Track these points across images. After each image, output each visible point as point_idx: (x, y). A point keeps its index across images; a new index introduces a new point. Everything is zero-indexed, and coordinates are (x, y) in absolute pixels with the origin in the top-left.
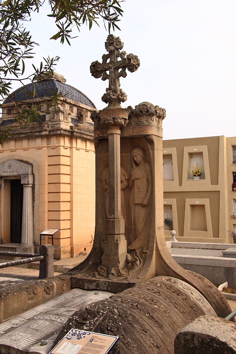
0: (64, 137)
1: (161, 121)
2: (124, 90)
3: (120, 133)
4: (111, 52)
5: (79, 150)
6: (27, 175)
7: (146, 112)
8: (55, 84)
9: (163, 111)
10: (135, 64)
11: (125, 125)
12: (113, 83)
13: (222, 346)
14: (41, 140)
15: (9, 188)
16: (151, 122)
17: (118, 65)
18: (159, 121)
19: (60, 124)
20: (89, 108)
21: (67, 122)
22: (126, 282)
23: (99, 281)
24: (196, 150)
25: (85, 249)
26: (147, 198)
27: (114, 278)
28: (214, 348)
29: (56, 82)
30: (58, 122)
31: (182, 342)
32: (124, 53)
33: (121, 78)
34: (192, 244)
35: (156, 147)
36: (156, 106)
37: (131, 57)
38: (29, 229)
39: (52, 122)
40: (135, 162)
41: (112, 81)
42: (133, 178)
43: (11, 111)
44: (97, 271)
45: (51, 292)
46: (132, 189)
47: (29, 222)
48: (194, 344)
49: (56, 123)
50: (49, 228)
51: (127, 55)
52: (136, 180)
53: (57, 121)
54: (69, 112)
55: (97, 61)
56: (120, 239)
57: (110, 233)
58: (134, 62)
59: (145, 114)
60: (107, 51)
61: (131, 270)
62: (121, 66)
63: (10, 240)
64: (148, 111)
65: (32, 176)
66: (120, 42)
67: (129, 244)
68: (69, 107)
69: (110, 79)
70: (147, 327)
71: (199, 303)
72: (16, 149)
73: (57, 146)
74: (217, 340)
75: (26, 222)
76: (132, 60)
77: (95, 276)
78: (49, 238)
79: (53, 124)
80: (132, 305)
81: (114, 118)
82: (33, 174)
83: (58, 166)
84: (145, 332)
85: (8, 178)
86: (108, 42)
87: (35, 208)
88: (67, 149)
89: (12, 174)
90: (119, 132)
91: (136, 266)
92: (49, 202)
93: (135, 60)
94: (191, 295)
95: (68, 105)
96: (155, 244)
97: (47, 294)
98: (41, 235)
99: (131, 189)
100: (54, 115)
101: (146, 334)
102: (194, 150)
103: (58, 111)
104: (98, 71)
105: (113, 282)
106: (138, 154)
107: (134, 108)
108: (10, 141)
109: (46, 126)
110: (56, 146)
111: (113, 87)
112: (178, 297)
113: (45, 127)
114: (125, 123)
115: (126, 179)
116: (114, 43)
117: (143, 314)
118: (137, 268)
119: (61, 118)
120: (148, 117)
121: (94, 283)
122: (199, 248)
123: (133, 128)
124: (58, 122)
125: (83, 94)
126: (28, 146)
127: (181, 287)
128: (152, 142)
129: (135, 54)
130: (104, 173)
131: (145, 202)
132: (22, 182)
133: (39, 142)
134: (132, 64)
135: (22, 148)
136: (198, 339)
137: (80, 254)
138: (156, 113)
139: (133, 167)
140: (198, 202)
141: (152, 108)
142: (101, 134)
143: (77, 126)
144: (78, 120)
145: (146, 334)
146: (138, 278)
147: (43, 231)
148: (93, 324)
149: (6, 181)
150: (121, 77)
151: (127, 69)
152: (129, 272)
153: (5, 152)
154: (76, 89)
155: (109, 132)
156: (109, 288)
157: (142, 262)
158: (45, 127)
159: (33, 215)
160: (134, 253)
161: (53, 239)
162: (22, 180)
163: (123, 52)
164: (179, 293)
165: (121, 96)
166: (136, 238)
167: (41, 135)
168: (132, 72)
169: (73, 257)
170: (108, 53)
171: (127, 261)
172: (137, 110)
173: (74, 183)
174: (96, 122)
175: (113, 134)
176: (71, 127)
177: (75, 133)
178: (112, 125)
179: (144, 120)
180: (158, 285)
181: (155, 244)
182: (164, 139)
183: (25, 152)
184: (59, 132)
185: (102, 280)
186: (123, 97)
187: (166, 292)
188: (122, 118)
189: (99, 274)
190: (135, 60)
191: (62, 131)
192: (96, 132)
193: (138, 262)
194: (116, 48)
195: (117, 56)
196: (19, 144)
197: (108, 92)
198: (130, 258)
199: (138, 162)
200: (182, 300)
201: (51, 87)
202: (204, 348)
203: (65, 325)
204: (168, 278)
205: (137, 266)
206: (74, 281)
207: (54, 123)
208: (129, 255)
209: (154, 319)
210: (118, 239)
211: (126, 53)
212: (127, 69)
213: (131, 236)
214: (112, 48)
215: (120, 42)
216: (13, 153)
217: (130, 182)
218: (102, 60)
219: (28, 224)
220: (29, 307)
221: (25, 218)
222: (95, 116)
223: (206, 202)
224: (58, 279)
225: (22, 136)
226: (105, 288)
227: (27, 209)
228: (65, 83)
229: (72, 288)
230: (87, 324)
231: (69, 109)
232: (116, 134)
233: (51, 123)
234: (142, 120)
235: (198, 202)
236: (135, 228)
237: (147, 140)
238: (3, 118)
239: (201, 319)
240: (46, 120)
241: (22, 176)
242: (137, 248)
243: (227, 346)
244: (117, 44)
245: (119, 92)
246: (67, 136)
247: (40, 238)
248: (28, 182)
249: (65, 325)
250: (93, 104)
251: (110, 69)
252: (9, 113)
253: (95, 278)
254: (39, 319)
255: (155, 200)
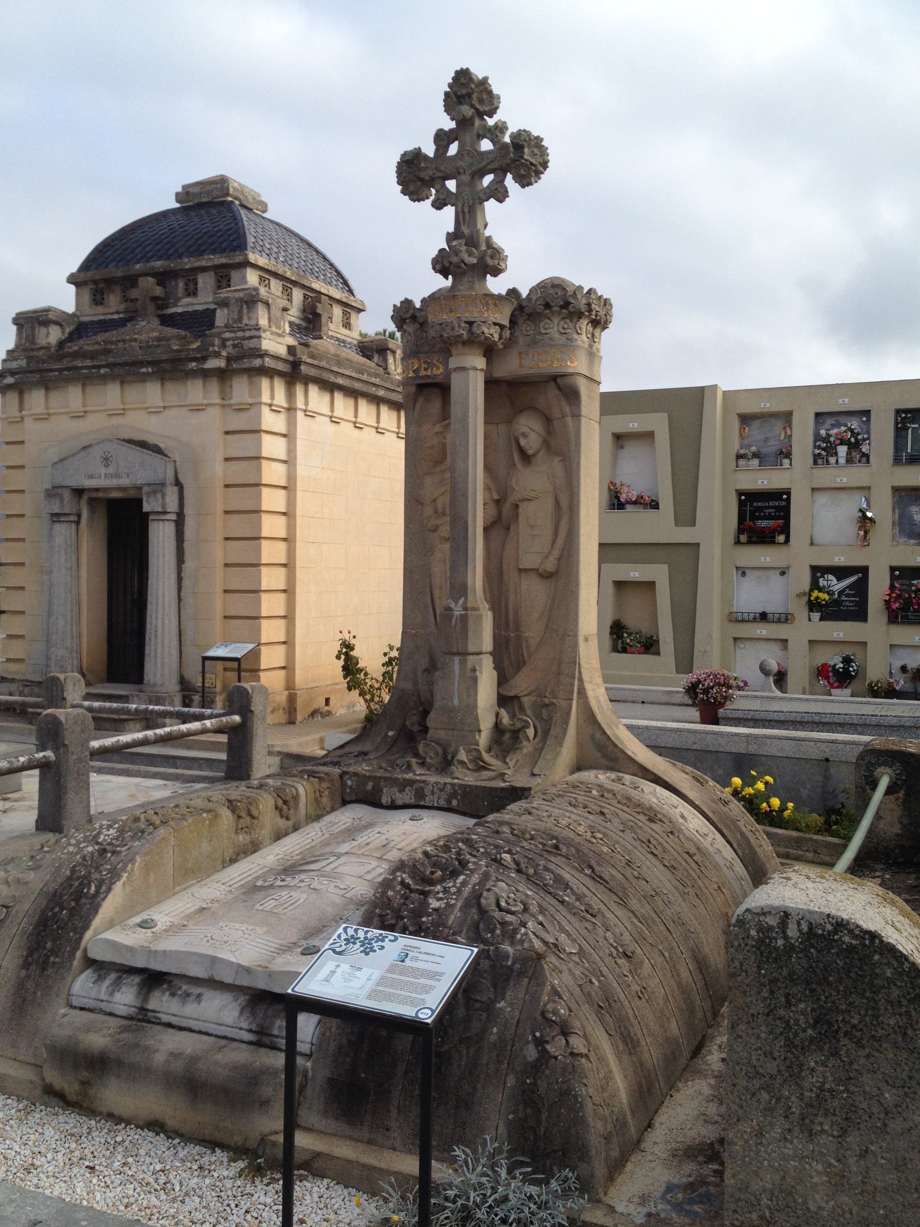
0: (271, 378)
1: (597, 334)
2: (499, 241)
3: (485, 368)
4: (463, 123)
5: (313, 417)
6: (158, 487)
7: (562, 307)
8: (238, 217)
9: (605, 305)
10: (533, 161)
11: (501, 346)
12: (467, 219)
13: (867, 942)
14: (204, 385)
15: (102, 525)
16: (576, 336)
17: (484, 163)
18: (593, 335)
19: (259, 337)
20: (337, 294)
21: (280, 332)
22: (503, 785)
23: (424, 782)
24: (636, 425)
25: (327, 701)
26: (556, 553)
27: (466, 775)
28: (844, 946)
29: (243, 212)
30: (254, 333)
31: (753, 933)
32: (501, 128)
33: (491, 205)
34: (624, 689)
35: (584, 410)
36: (590, 290)
37: (525, 141)
38: (166, 641)
39: (235, 332)
40: (522, 452)
41: (466, 210)
42: (512, 498)
43: (103, 294)
44: (416, 755)
45: (292, 811)
46: (512, 528)
47: (166, 622)
48: (786, 937)
49: (248, 334)
50: (226, 642)
51: (512, 133)
52: (526, 503)
53: (250, 330)
54: (284, 303)
55: (419, 148)
56: (481, 666)
57: (455, 650)
58: (534, 155)
59: (559, 313)
60: (452, 119)
61: (512, 753)
62: (490, 167)
63: (105, 676)
64: (566, 304)
65: (176, 489)
66: (490, 93)
67: (502, 680)
68: (281, 289)
69: (460, 205)
70: (596, 904)
71: (706, 843)
72: (124, 409)
73: (250, 405)
74: (852, 927)
75: (160, 621)
76: (526, 150)
77: (409, 767)
78: (225, 669)
79: (237, 338)
80: (544, 845)
81: (471, 323)
82: (178, 483)
83: (255, 462)
84: (592, 915)
85: (100, 495)
86: (455, 94)
87: (186, 583)
88: (279, 412)
89: (114, 482)
90: (480, 362)
91: (525, 743)
92: (226, 565)
93: (536, 151)
94: (681, 820)
95: (277, 281)
96: (576, 682)
97: (282, 817)
98: (205, 659)
99: (508, 529)
100: (240, 312)
101: (593, 920)
102: (631, 425)
103: (251, 300)
104: (422, 180)
105: (465, 786)
106: (533, 430)
107: (418, 305)
108: (31, 389)
109: (217, 341)
110: (246, 404)
111: (466, 230)
112: (654, 826)
113: (213, 345)
114: (500, 338)
115: (494, 501)
116: (474, 96)
117: (576, 868)
118: (527, 748)
119: (263, 322)
120: (568, 321)
121: (412, 787)
122: (643, 702)
123: (520, 354)
124: (254, 333)
125: (317, 252)
126: (84, 406)
127: (655, 800)
128: (572, 396)
129: (535, 133)
130: (428, 481)
131: (550, 566)
132: (146, 508)
133: (195, 391)
134: (526, 160)
135: (145, 406)
136: (799, 924)
137: (313, 714)
138: (590, 310)
139: (514, 465)
140: (637, 574)
141: (579, 297)
142: (426, 369)
143: (306, 345)
144: (306, 329)
145: (593, 920)
146: (534, 775)
147: (209, 648)
148: (454, 894)
149: (92, 502)
150: (492, 200)
151: (509, 176)
152: (506, 757)
153: (91, 418)
154: (296, 235)
155: (453, 363)
156: (455, 803)
157: (539, 733)
158: (213, 345)
159: (179, 603)
160: (517, 708)
161: (239, 670)
162: (148, 501)
163: (500, 124)
164: (653, 816)
165: (492, 257)
166: (520, 664)
167: (203, 369)
168: (523, 186)
169: (294, 723)
170: (452, 125)
171: (498, 728)
172: (537, 300)
173: (299, 512)
174: (409, 334)
175: (463, 369)
176: (291, 350)
177: (302, 367)
178: (464, 343)
179: (553, 327)
180: (594, 792)
181: (576, 682)
182: (605, 388)
183: (154, 419)
184: (257, 362)
185: (433, 779)
186: (496, 262)
187: (620, 812)
188: (495, 324)
189: (423, 764)
190: (536, 151)
191: (267, 359)
192: (410, 362)
193: (531, 732)
194: (477, 110)
195: (480, 137)
196: (56, 397)
197: (454, 243)
198: (506, 720)
199: (530, 452)
200: (664, 835)
201: (228, 224)
202: (816, 949)
203: (376, 897)
204: (613, 775)
205: (528, 740)
206: (349, 783)
207: (240, 334)
208: (503, 712)
209: (607, 882)
210: (477, 668)
211: (507, 129)
212: (509, 176)
213: (505, 660)
214: (466, 110)
215: (491, 92)
216: (115, 421)
217: (507, 508)
218: (433, 147)
219: (163, 627)
220: (238, 854)
221: (157, 611)
222: (409, 315)
223: (658, 573)
224: (306, 777)
225: (144, 370)
226: (442, 803)
227: (160, 583)
228: (264, 215)
229: (345, 803)
230: (438, 893)
231: (279, 294)
232: (475, 369)
233: (233, 335)
234: (550, 331)
235: (637, 574)
236: (519, 637)
237: (559, 388)
238: (78, 313)
239: (791, 875)
240: (217, 324)
241: (145, 489)
242: (525, 693)
243: (882, 941)
244: (483, 100)
245: (483, 248)
246: (281, 374)
247: (201, 670)
248: (163, 506)
249: (376, 897)
250: (345, 283)
251: (459, 173)
252: (98, 299)
253: (411, 775)
254: (272, 885)
255: (577, 562)
